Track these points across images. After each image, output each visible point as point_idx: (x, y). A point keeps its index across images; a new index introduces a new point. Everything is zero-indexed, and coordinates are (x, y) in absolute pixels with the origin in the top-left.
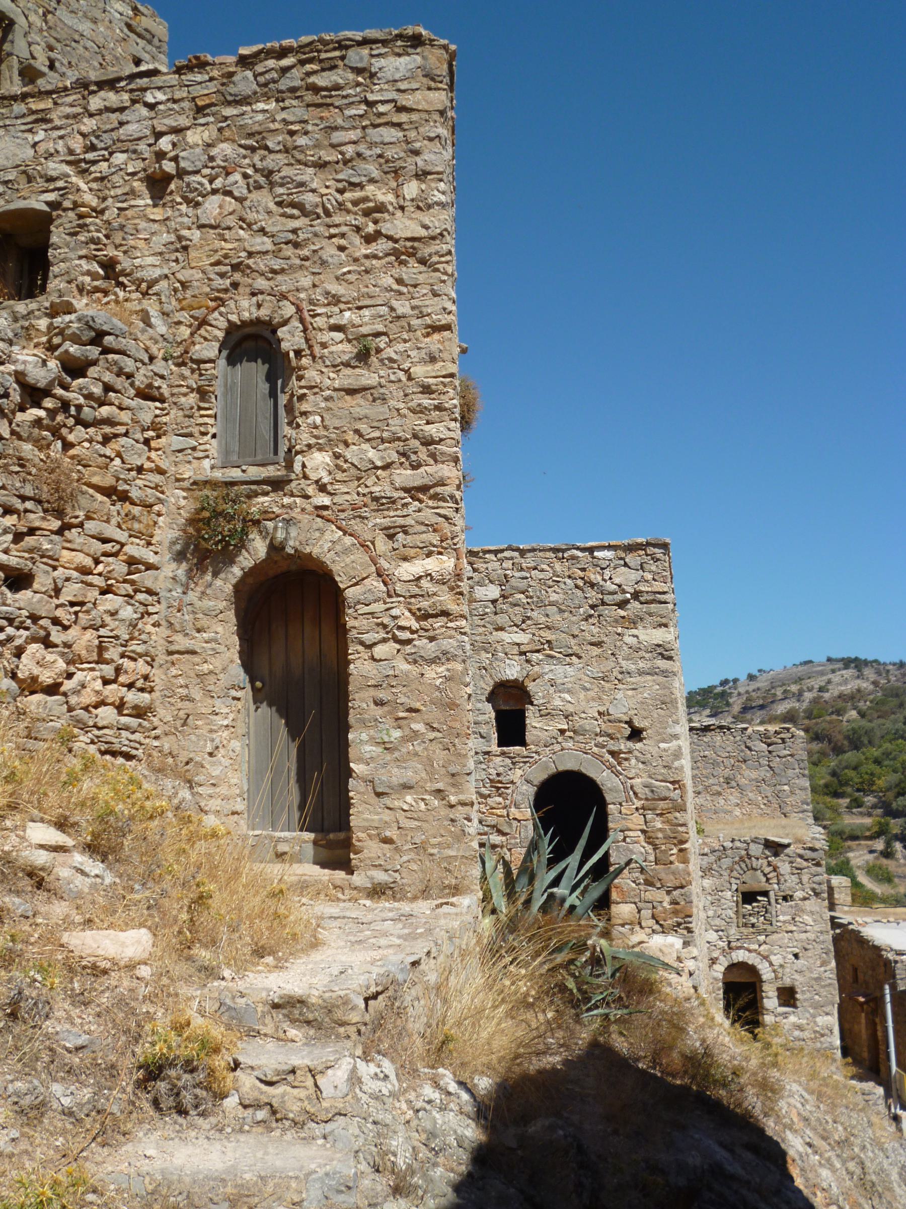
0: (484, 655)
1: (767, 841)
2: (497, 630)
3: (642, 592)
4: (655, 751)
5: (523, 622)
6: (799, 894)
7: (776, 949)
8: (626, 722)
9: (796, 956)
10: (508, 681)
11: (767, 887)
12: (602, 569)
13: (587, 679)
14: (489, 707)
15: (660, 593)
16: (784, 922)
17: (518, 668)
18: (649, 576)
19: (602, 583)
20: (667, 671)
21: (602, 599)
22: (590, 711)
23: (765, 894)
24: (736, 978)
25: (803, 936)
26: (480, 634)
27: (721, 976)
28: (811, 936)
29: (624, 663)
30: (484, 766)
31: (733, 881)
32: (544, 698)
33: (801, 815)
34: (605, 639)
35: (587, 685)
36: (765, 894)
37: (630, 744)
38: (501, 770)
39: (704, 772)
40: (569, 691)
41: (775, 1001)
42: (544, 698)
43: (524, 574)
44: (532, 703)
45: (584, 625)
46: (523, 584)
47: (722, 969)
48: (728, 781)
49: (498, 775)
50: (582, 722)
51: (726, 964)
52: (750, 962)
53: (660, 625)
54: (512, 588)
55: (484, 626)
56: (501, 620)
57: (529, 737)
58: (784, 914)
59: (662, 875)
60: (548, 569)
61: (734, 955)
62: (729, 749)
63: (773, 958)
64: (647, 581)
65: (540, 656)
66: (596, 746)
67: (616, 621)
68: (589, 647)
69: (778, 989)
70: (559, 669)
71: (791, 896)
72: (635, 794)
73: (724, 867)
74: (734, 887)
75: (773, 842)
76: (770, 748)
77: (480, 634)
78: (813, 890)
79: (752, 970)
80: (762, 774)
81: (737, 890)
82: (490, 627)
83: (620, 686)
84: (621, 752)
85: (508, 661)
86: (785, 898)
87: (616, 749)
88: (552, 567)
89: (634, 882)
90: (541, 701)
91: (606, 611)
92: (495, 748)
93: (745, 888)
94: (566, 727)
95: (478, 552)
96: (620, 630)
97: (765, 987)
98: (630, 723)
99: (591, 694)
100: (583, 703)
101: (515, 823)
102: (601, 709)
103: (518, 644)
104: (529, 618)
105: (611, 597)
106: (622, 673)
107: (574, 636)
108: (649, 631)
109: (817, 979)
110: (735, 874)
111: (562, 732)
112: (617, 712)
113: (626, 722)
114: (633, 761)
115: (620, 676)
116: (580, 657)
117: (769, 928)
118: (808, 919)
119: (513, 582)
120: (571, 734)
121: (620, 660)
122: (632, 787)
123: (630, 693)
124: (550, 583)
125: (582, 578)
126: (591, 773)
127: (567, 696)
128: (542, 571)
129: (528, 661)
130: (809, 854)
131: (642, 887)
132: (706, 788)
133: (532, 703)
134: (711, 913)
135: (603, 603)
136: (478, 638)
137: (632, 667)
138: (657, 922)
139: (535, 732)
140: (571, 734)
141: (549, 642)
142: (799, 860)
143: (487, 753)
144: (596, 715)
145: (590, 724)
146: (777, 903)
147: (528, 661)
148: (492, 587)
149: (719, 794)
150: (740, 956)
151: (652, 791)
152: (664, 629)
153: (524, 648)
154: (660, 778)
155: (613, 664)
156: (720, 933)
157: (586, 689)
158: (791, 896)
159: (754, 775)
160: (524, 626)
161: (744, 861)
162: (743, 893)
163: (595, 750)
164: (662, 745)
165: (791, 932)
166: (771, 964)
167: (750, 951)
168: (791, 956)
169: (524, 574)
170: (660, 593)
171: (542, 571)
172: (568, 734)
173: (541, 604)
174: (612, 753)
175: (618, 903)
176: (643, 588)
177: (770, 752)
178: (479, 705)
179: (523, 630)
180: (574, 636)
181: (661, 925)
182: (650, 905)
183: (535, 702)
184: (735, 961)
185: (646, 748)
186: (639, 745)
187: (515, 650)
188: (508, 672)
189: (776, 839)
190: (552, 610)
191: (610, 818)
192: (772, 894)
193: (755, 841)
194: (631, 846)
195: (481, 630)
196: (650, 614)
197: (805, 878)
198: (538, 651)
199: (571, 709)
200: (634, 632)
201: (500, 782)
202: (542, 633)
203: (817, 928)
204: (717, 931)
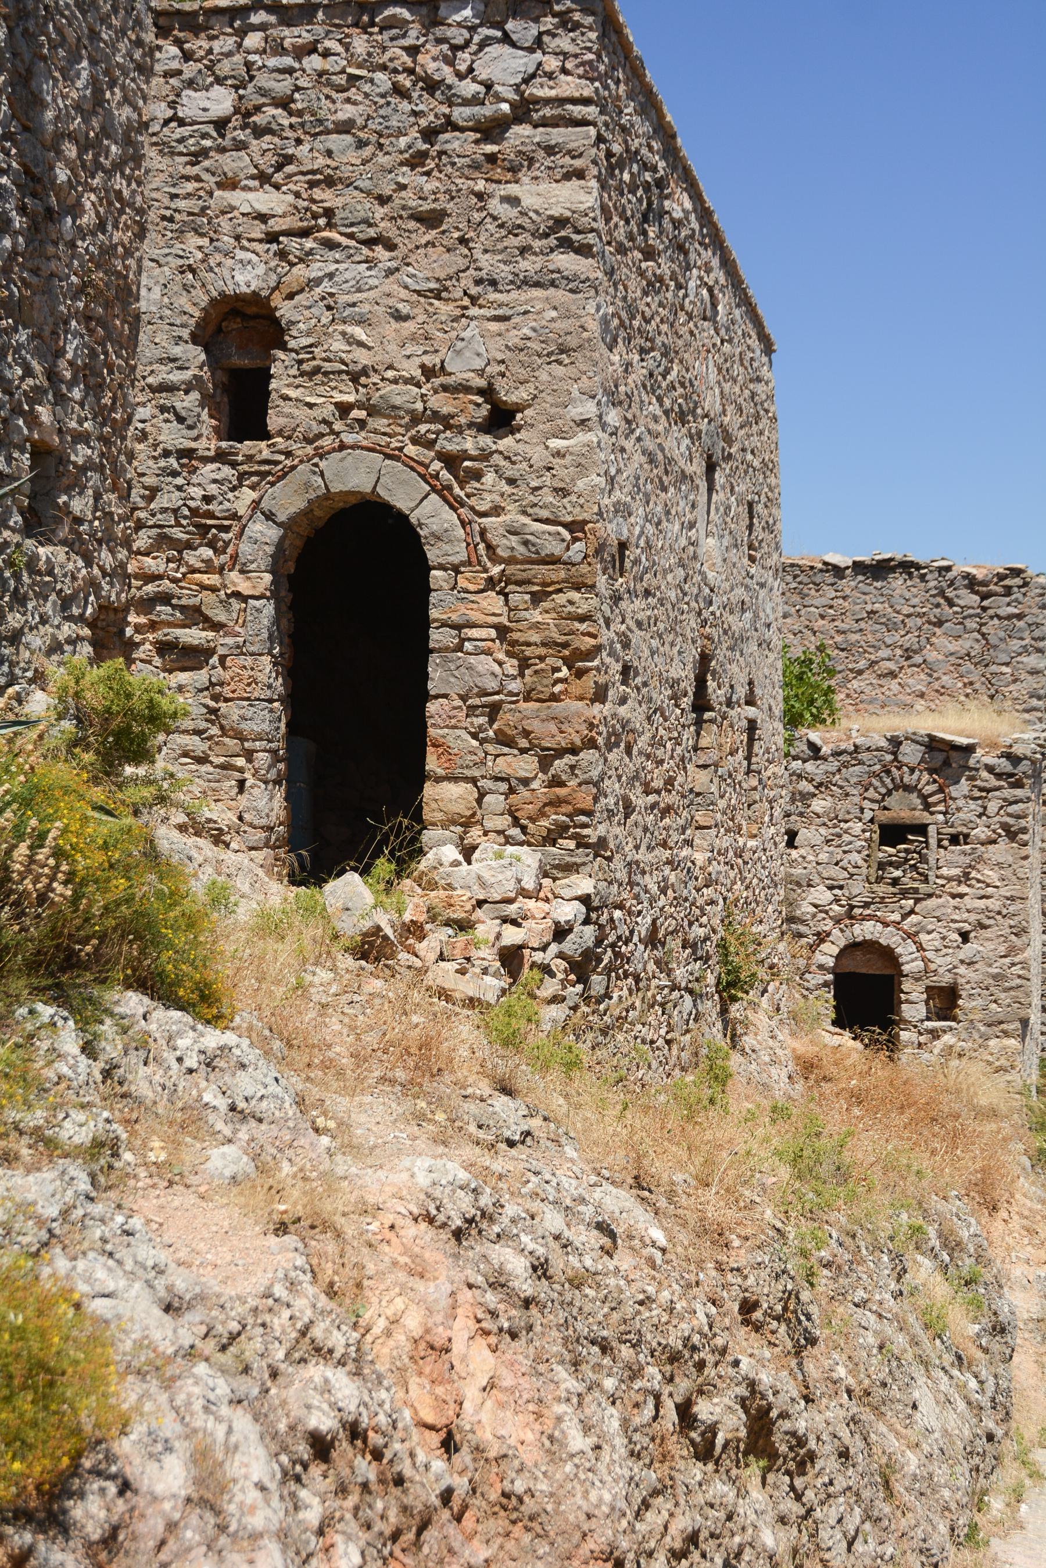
0: (193, 241)
1: (932, 738)
2: (220, 185)
3: (537, 101)
4: (538, 456)
5: (279, 167)
6: (980, 832)
7: (931, 924)
8: (480, 392)
9: (965, 937)
10: (238, 298)
11: (926, 818)
12: (455, 48)
13: (404, 294)
14: (197, 355)
15: (574, 101)
16: (949, 879)
17: (261, 269)
18: (552, 63)
19: (451, 79)
20: (575, 278)
21: (447, 117)
22: (405, 364)
23: (921, 829)
24: (861, 965)
25: (982, 904)
26: (188, 196)
27: (831, 962)
28: (994, 904)
29: (485, 261)
30: (179, 481)
31: (866, 804)
32: (309, 334)
33: (1026, 716)
34: (450, 206)
35: (404, 309)
36: (921, 829)
37: (485, 440)
38: (213, 489)
39: (870, 637)
40: (362, 321)
41: (922, 1011)
42: (309, 334)
43: (288, 61)
44: (283, 347)
45: (406, 174)
46: (282, 86)
47: (835, 951)
48: (908, 653)
49: (207, 499)
50: (387, 389)
51: (842, 943)
52: (883, 941)
53: (567, 177)
54: (262, 92)
55: (198, 179)
56: (232, 163)
57: (274, 421)
58: (950, 864)
59: (534, 725)
60: (339, 49)
61: (857, 929)
62: (915, 601)
63: (923, 937)
64: (550, 76)
65: (309, 244)
66: (415, 441)
67: (475, 166)
68: (412, 225)
69: (929, 989)
70: (352, 271)
71: (966, 836)
72: (489, 547)
73: (853, 780)
74: (868, 815)
75: (943, 741)
76: (985, 603)
77: (188, 196)
78: (1005, 827)
79: (888, 955)
80: (967, 644)
81: (872, 821)
82: (211, 180)
83: (474, 311)
84: (465, 455)
85: (240, 255)
86: (954, 840)
87: (451, 447)
88: (347, 47)
89: (474, 736)
90: (305, 341)
91: (454, 142)
92: (207, 445)
93: (884, 817)
94: (351, 398)
95: (194, 14)
96: (480, 186)
97: (906, 986)
98: (488, 392)
99: (410, 326)
100: (393, 348)
101: (236, 605)
102: (429, 360)
103: (263, 218)
104: (289, 159)
105: (467, 111)
106: (478, 282)
107: (383, 200)
108: (543, 187)
109: (995, 977)
110: (871, 793)
111: (344, 409)
112: (461, 369)
113: (480, 392)
114: (489, 478)
115: (474, 291)
116: (391, 246)
117: (923, 888)
118: (991, 875)
119: (263, 80)
120: (362, 414)
121: (478, 254)
122: (483, 533)
123: (494, 326)
124: (341, 80)
125: (411, 72)
126: (401, 502)
127: (359, 332)
128: (326, 54)
129: (282, 255)
130: (1005, 765)
131: (490, 748)
132: (873, 663)
133: (283, 347)
134: (823, 857)
135: (450, 125)
136: (181, 204)
137: (504, 272)
138: (516, 822)
139: (287, 408)
140: (362, 414)
141: (329, 213)
142: (985, 774)
143: (187, 453)
144: (417, 373)
145: (403, 396)
146: (940, 846)
147: (282, 255)
148: (217, 91)
149: (893, 675)
150: (866, 930)
151: (526, 543)
152: (575, 183)
153: (276, 225)
154: (545, 514)
155: (462, 263)
156: (837, 891)
157: (399, 317)
158: (966, 836)
159: (953, 646)
160: (278, 177)
161: (888, 772)
162: (882, 827)
163: (411, 450)
164: (555, 443)
165: (961, 896)
166: (921, 948)
167: (886, 924)
168: (956, 936)
169: (288, 61)
170: (574, 101)
171: (326, 54)
172: (356, 413)
173: (320, 129)
174: (451, 461)
175: (439, 780)
176: (540, 90)
177: (984, 609)
178: (177, 351)
179: (277, 187)
180: (383, 200)
181: (524, 829)
182: (504, 787)
183: (292, 344)
184: (860, 939)
185: (520, 447)
186: (507, 443)
187: (258, 230)
188: (240, 278)
189: (948, 737)
190: (337, 141)
191: (433, 598)
192: (932, 830)
193: (913, 739)
194: (472, 659)
195: (190, 187)
196: (550, 150)
197: (993, 806)
198: (305, 233)
199: (363, 357)
200: (513, 189)
201: (210, 515)
202: (317, 193)
203: (1005, 892)
204: (831, 888)
